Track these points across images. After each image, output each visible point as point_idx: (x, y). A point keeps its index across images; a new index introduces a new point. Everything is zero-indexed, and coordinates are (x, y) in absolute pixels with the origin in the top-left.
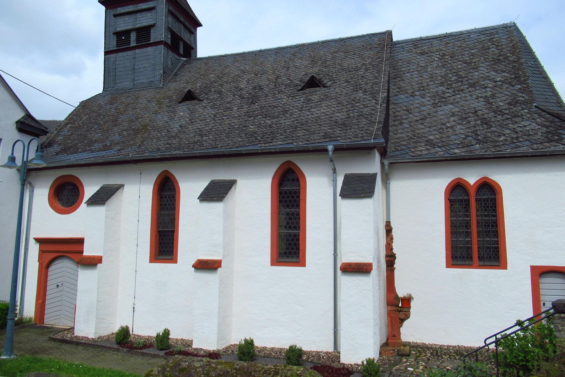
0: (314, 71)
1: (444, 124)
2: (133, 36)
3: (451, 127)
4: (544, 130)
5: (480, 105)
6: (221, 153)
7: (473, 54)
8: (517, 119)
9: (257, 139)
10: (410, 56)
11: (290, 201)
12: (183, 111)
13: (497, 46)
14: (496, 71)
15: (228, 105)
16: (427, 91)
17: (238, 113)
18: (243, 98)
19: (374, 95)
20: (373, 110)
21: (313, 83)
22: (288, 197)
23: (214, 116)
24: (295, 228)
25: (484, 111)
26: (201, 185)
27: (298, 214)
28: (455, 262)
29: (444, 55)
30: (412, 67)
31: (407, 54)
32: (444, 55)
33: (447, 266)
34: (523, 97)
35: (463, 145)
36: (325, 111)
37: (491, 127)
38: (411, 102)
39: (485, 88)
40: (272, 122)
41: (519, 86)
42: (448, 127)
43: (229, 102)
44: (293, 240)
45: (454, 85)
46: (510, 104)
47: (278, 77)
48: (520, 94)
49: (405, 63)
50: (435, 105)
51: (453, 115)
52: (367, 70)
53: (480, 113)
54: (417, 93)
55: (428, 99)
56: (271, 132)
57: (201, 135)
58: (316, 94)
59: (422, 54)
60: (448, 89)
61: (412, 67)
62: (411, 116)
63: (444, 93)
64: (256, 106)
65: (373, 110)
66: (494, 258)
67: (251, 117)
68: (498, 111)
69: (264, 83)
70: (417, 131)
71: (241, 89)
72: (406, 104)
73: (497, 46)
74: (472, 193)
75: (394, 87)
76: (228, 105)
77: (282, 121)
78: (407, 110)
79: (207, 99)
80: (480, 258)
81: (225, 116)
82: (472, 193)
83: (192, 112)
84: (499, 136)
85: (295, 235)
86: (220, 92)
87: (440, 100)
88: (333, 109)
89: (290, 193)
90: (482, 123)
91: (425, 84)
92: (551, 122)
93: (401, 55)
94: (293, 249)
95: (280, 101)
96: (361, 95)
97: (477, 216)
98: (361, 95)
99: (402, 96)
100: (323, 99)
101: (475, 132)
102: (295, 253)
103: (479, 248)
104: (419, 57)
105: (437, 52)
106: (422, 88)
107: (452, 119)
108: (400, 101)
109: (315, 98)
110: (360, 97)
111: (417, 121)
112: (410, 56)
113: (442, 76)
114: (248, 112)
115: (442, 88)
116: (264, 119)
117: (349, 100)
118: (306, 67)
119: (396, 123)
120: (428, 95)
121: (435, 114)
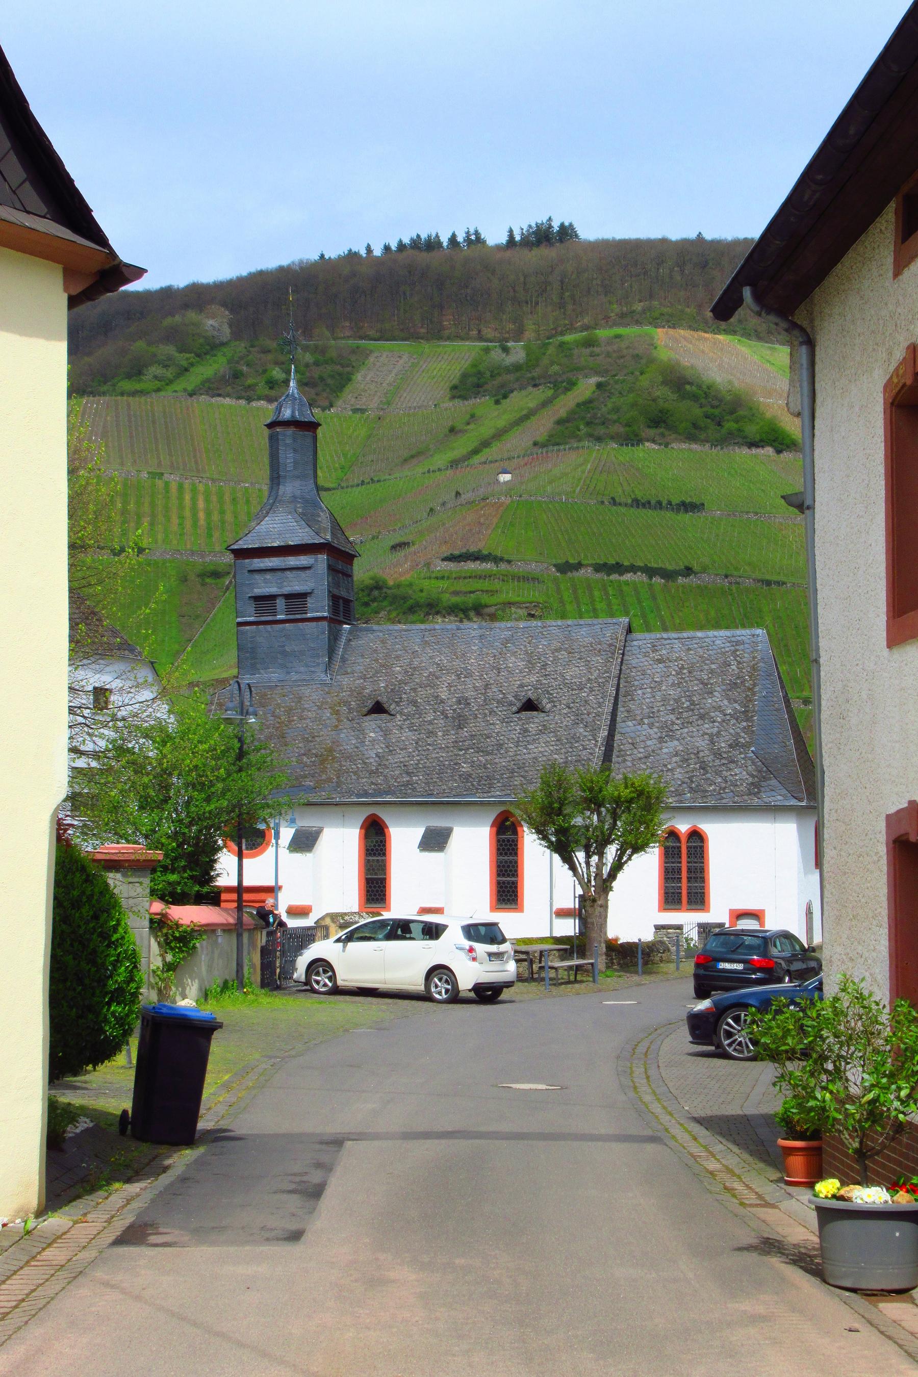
0: (531, 695)
1: (665, 766)
2: (280, 603)
3: (671, 770)
4: (751, 780)
5: (702, 743)
6: (733, 1001)
7: (712, 671)
8: (732, 766)
9: (473, 785)
10: (646, 663)
11: (508, 849)
12: (372, 727)
13: (739, 663)
14: (729, 700)
15: (430, 728)
16: (657, 719)
17: (445, 742)
18: (447, 717)
19: (594, 732)
20: (591, 754)
21: (530, 706)
22: (506, 845)
23: (416, 743)
24: (513, 875)
25: (706, 754)
26: (416, 833)
27: (516, 862)
28: (667, 907)
29: (682, 668)
30: (646, 681)
31: (643, 660)
32: (682, 668)
33: (660, 911)
34: (744, 738)
35: (678, 793)
36: (543, 750)
37: (707, 772)
38: (638, 733)
39: (714, 722)
40: (486, 760)
41: (745, 724)
42: (668, 770)
43: (430, 723)
44: (511, 887)
45: (685, 715)
46: (730, 746)
47: (487, 686)
48: (743, 734)
49: (639, 673)
50: (661, 740)
51: (676, 755)
52: (591, 690)
53: (701, 754)
54: (646, 721)
55: (656, 730)
56: (487, 776)
57: (408, 773)
58: (535, 721)
59: (660, 661)
60: (678, 719)
61: (646, 681)
62: (635, 751)
63: (673, 723)
64: (465, 733)
65: (591, 754)
66: (501, 871)
67: (461, 750)
68: (718, 754)
69: (470, 694)
70: (639, 772)
71: (442, 701)
72: (632, 735)
73: (739, 663)
74: (684, 839)
75: (622, 709)
76: (430, 728)
77: (497, 760)
78: (633, 744)
79: (401, 714)
80: (690, 902)
81: (429, 745)
82: (684, 839)
83: (386, 733)
84: (711, 785)
85: (513, 883)
86: (414, 703)
87: (668, 733)
88: (551, 748)
89: (508, 841)
90: (701, 768)
91: (655, 710)
92: (760, 771)
93: (636, 660)
94: (511, 896)
95: (492, 727)
96: (582, 730)
97: (688, 862)
98: (582, 730)
99: (630, 723)
100: (540, 731)
101: (690, 778)
102: (513, 900)
103: (689, 893)
104: (655, 666)
105: (676, 661)
106: (652, 715)
107: (674, 759)
108: (628, 730)
109: (532, 727)
110: (581, 734)
111: (640, 759)
112: (646, 663)
113: (626, 778)
114: (456, 742)
115: (672, 716)
116: (477, 755)
117: (569, 737)
118: (521, 672)
119: (620, 759)
120: (657, 724)
121: (659, 752)
